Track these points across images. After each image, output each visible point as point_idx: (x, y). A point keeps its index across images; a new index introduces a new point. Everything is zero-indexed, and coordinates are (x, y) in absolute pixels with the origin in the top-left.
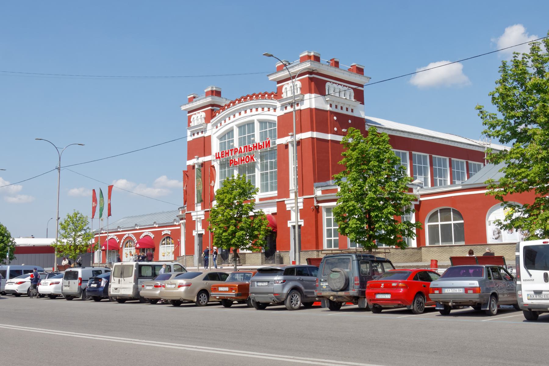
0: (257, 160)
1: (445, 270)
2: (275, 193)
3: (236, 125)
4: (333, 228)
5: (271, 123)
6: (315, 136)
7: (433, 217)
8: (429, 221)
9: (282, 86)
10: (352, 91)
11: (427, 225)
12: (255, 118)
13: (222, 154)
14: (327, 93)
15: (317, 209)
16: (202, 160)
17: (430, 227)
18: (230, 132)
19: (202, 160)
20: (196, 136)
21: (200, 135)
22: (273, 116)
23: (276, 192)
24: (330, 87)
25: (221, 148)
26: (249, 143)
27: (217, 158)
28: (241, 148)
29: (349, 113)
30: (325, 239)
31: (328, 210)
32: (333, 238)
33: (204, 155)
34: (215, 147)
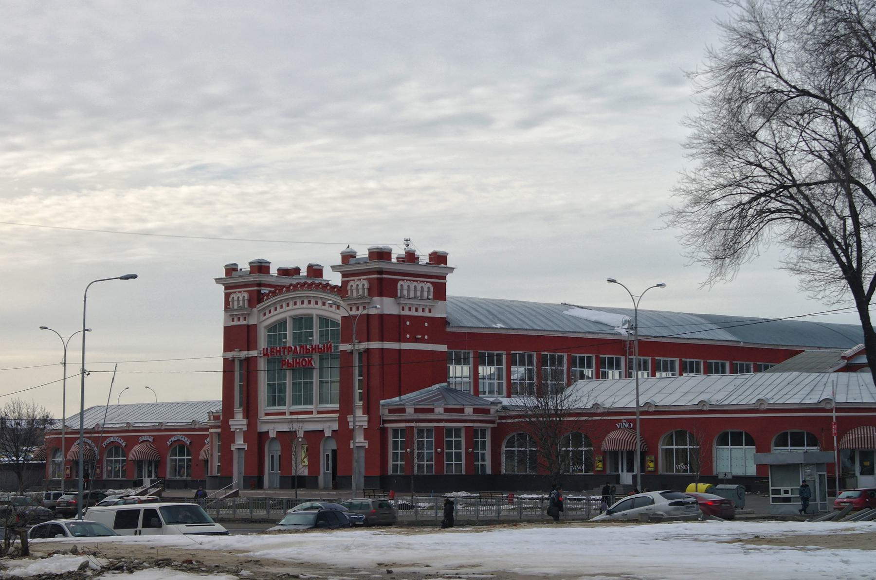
0: (316, 363)
1: (866, 293)
2: (336, 406)
3: (291, 317)
4: (399, 463)
5: (334, 323)
6: (387, 311)
7: (510, 444)
8: (507, 447)
9: (349, 281)
10: (430, 285)
11: (504, 449)
12: (315, 313)
13: (271, 351)
14: (399, 295)
15: (384, 431)
16: (244, 354)
17: (507, 452)
18: (282, 324)
19: (244, 354)
20: (236, 323)
21: (242, 322)
22: (337, 315)
23: (338, 405)
24: (404, 285)
25: (269, 342)
26: (306, 340)
27: (264, 355)
28: (296, 348)
29: (427, 314)
30: (391, 463)
31: (395, 431)
32: (399, 463)
33: (248, 350)
34: (263, 342)
